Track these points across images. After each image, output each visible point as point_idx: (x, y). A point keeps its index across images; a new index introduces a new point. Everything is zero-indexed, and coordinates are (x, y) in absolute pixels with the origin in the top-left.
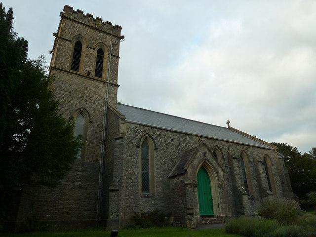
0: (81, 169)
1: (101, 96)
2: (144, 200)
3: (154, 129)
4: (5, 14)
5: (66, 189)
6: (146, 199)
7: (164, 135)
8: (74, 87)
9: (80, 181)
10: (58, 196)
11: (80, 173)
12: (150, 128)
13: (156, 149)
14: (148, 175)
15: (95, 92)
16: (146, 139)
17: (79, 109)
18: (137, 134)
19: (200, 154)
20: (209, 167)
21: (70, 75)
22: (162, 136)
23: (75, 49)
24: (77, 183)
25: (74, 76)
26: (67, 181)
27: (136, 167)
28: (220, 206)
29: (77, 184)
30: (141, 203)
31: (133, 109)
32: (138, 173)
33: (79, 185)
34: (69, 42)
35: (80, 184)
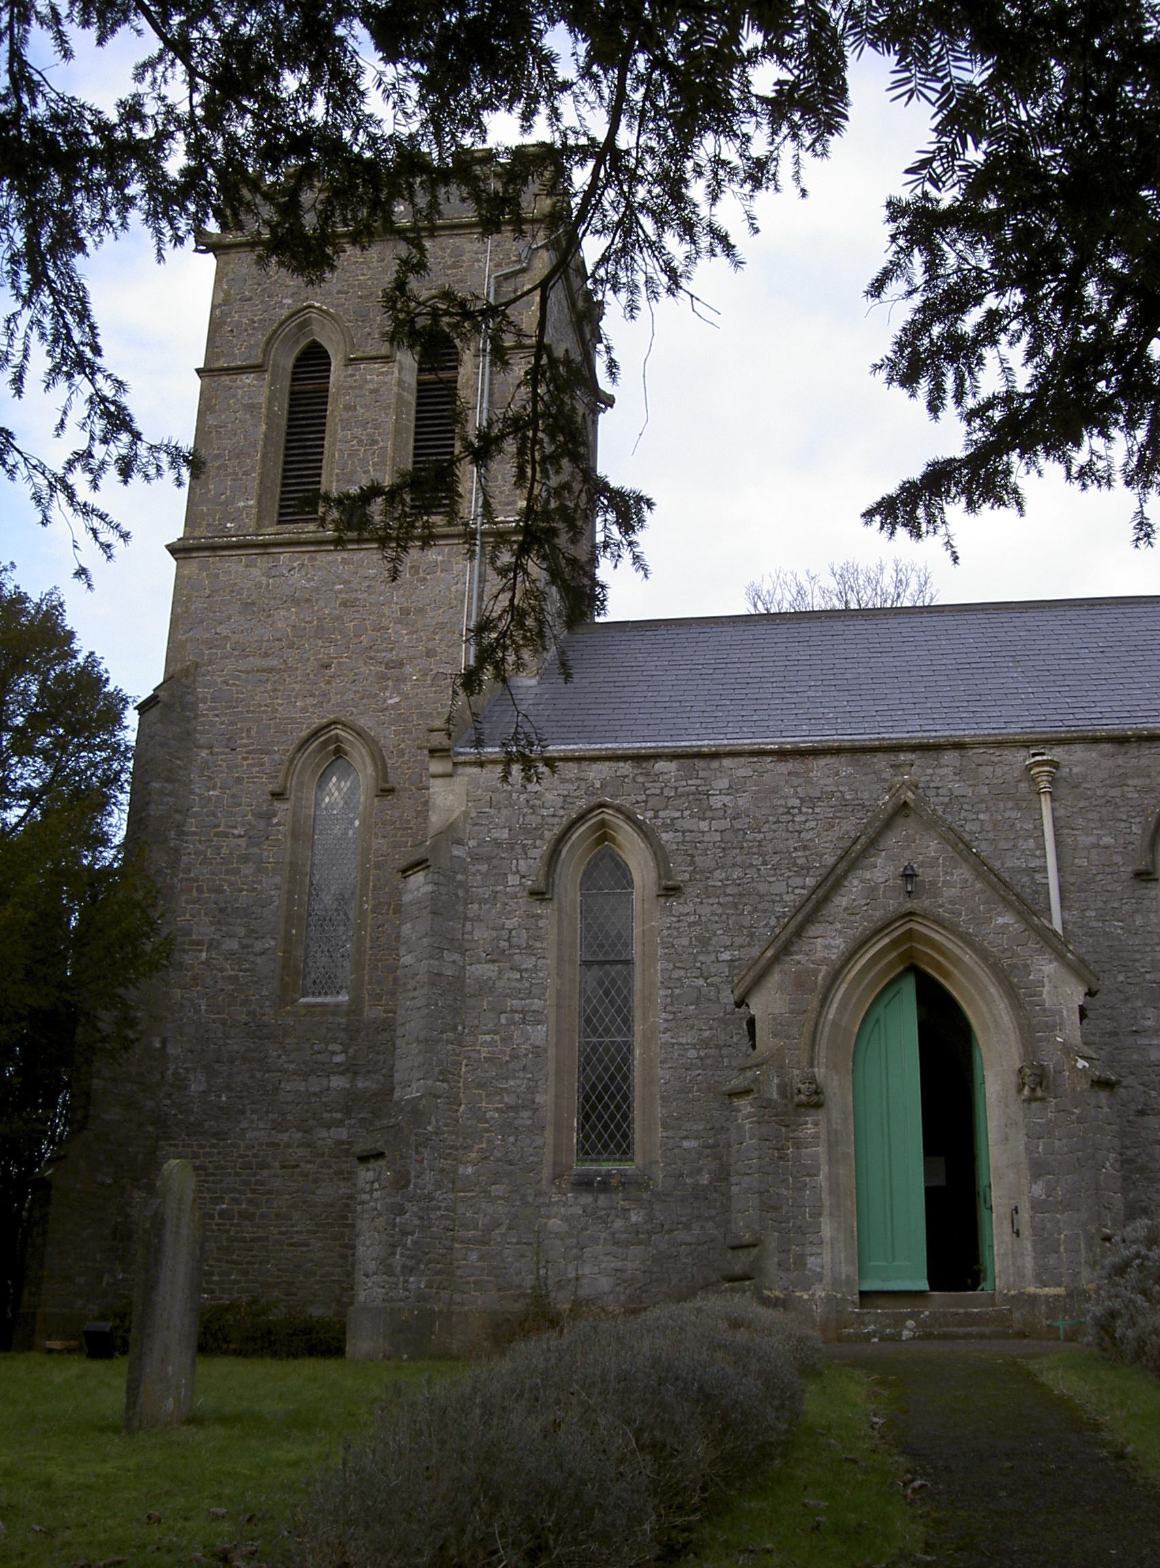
0: (339, 1058)
1: (441, 625)
2: (576, 1204)
3: (661, 766)
4: (641, 212)
5: (276, 1164)
6: (587, 1199)
7: (731, 790)
8: (285, 619)
9: (340, 1123)
10: (236, 1201)
11: (338, 1082)
12: (626, 768)
13: (670, 891)
14: (630, 1050)
15: (405, 612)
16: (603, 835)
17: (315, 734)
18: (534, 820)
19: (871, 891)
20: (957, 962)
21: (263, 563)
22: (716, 802)
23: (295, 398)
24: (323, 1133)
25: (285, 557)
26: (277, 1127)
27: (529, 1017)
28: (1026, 1232)
29: (327, 1137)
30: (555, 1224)
31: (1004, 617)
32: (538, 1052)
33: (340, 1143)
34: (248, 379)
35: (344, 1137)
